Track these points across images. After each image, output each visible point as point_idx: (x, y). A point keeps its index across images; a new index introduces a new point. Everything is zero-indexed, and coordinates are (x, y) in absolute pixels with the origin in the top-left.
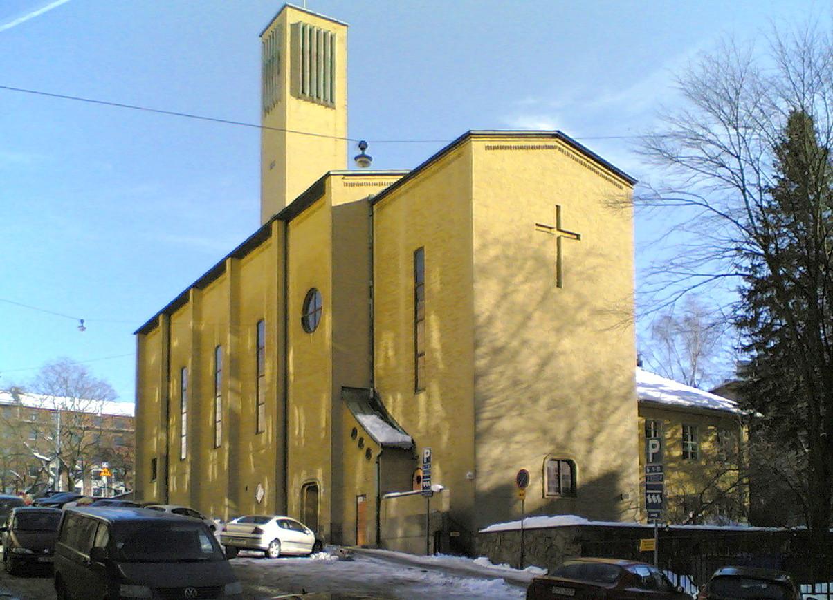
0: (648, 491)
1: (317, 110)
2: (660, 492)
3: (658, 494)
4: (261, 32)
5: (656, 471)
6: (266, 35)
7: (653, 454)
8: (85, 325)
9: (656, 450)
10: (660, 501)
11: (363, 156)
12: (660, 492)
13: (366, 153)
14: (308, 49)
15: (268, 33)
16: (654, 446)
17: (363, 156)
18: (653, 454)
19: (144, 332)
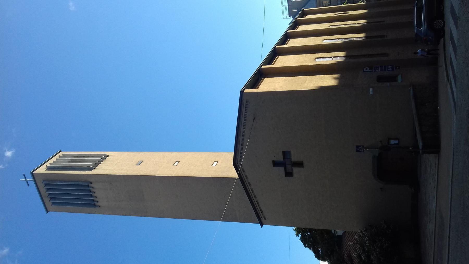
6: (49, 203)
9: (368, 68)
15: (47, 200)
16: (366, 69)
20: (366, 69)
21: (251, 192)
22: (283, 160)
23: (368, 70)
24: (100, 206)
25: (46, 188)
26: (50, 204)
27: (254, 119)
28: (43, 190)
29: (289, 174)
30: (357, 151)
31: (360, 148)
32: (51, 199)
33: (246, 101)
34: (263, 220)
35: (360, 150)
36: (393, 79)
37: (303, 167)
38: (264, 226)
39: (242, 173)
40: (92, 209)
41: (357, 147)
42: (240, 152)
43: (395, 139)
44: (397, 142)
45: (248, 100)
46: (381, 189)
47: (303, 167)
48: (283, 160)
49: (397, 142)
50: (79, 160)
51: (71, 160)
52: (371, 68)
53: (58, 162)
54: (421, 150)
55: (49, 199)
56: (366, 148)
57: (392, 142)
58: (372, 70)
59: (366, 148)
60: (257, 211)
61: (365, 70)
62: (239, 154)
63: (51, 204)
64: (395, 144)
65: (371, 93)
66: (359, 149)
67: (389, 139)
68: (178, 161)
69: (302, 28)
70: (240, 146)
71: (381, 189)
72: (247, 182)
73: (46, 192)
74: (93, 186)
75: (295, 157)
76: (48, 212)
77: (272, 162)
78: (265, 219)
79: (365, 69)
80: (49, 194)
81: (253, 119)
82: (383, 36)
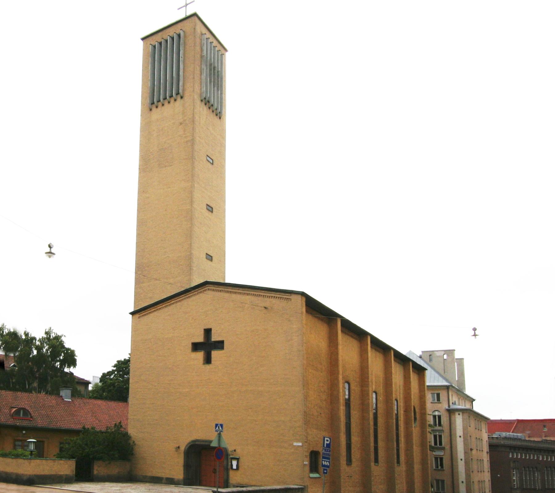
0: (323, 459)
1: (212, 443)
2: (329, 460)
3: (328, 461)
4: (208, 254)
5: (327, 451)
6: (154, 41)
7: (327, 444)
8: (473, 333)
9: (328, 442)
10: (328, 464)
11: (50, 253)
12: (329, 460)
13: (53, 251)
14: (396, 409)
15: (158, 38)
16: (327, 441)
17: (50, 253)
18: (327, 444)
19: (212, 208)
20: (327, 441)
21: (173, 302)
22: (213, 340)
23: (326, 442)
24: (151, 110)
25: (174, 35)
26: (153, 43)
27: (265, 308)
28: (171, 32)
29: (196, 347)
30: (216, 425)
31: (220, 428)
32: (159, 43)
33: (289, 299)
34: (137, 316)
35: (217, 428)
36: (314, 467)
37: (204, 364)
38: (131, 315)
39: (52, 488)
40: (148, 101)
41: (222, 425)
42: (223, 289)
43: (238, 466)
44: (235, 467)
45: (291, 300)
46: (179, 447)
47: (204, 364)
48: (213, 340)
49: (235, 467)
50: (214, 79)
51: (214, 68)
52: (328, 445)
53: (211, 49)
54: (217, 490)
55: (159, 41)
56: (220, 434)
57: (234, 463)
58: (325, 446)
59: (220, 434)
60: (149, 308)
61: (326, 439)
62: (221, 289)
63: (154, 45)
64: (232, 465)
65: (295, 444)
66: (219, 427)
67: (238, 459)
68: (212, 211)
69: (32, 458)
70: (230, 290)
71: (179, 447)
72: (183, 298)
73: (169, 37)
74: (177, 100)
75: (215, 354)
76: (143, 39)
77: (210, 328)
78: (139, 317)
79: (328, 439)
80: (167, 41)
81: (266, 307)
82: (376, 461)
